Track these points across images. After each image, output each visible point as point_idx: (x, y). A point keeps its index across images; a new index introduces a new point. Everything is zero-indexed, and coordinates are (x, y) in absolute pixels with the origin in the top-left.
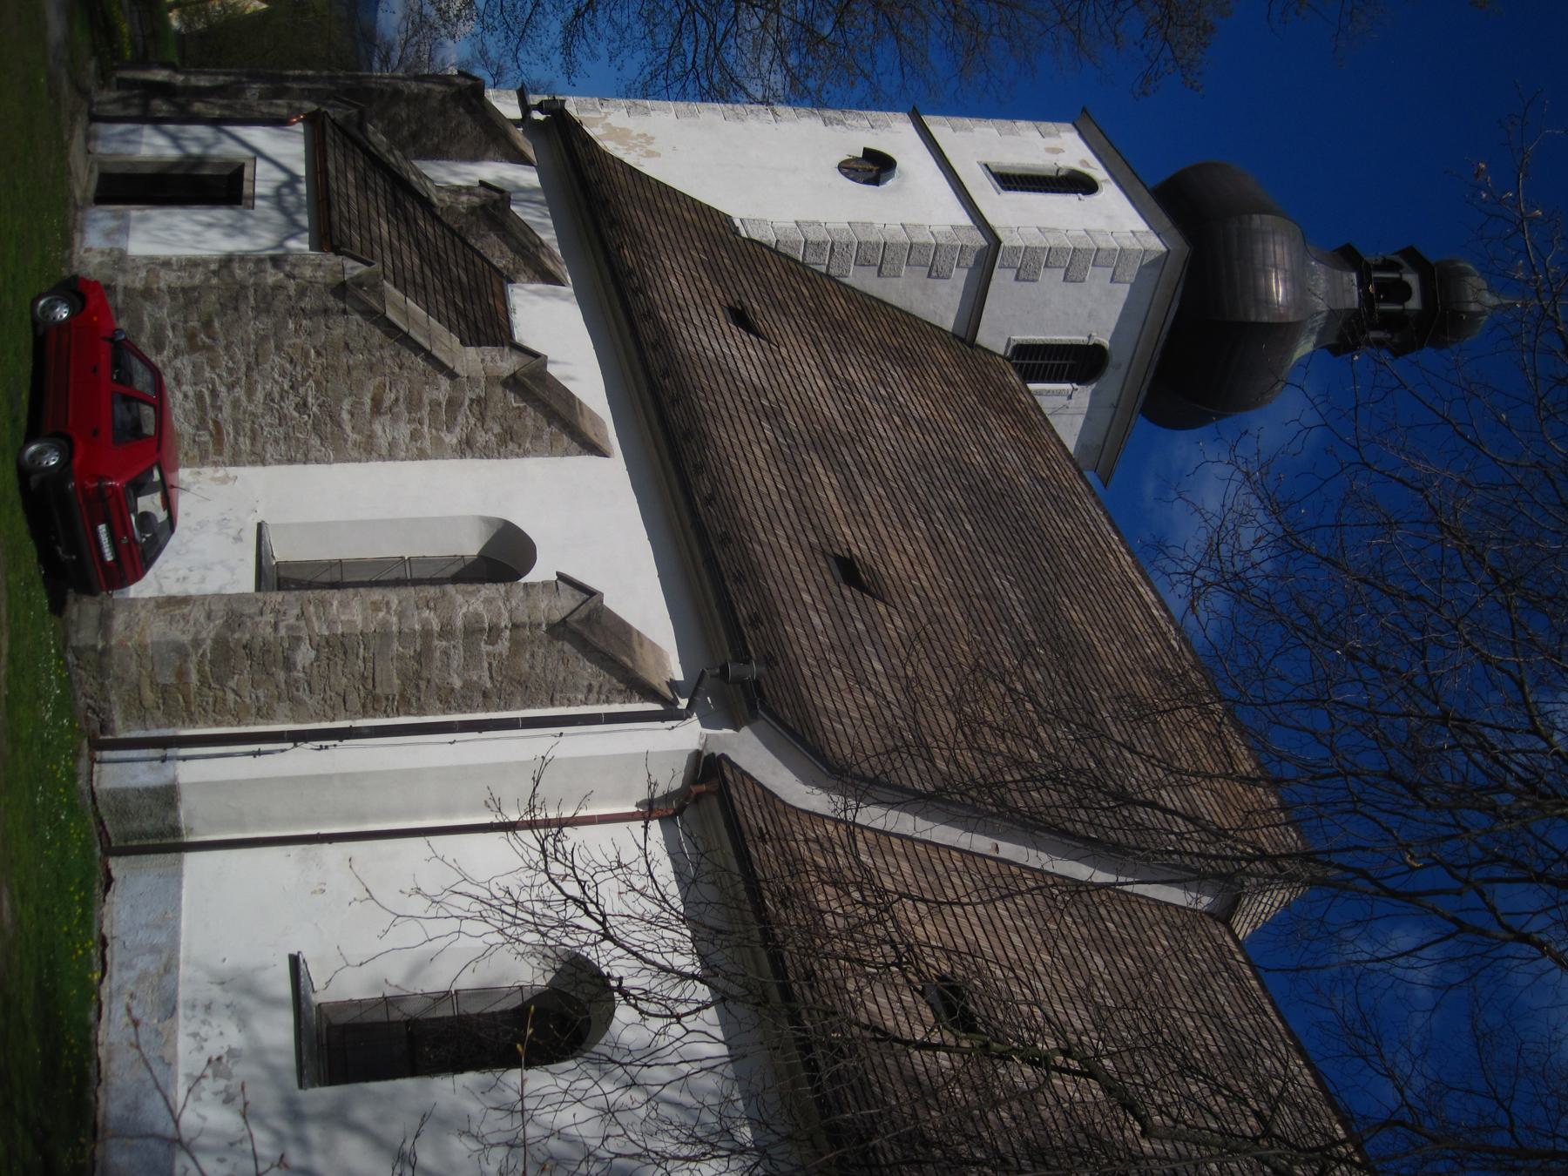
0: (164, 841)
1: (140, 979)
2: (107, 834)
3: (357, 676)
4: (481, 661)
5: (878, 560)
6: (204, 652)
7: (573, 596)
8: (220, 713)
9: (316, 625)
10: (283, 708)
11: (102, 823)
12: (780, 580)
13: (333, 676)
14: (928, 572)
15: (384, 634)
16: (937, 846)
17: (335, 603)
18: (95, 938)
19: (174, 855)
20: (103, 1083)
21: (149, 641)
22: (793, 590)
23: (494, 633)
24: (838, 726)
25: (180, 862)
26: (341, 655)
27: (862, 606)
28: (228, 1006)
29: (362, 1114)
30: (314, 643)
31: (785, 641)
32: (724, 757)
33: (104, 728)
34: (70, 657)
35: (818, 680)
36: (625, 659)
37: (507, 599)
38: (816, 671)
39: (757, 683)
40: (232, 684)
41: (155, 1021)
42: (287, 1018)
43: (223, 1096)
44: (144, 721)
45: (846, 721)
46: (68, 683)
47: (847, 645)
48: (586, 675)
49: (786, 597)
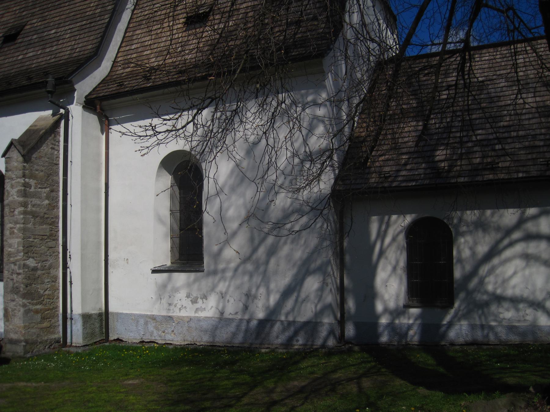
0: (104, 319)
1: (157, 329)
2: (100, 340)
3: (41, 242)
4: (38, 192)
5: (5, 26)
6: (28, 303)
7: (12, 151)
8: (54, 297)
9: (19, 258)
10: (52, 271)
11: (95, 343)
12: (11, 68)
13: (41, 252)
14: (13, 6)
15: (24, 230)
16: (131, 18)
17: (10, 249)
18: (141, 345)
19: (109, 316)
20: (196, 343)
21: (22, 325)
22: (17, 62)
23: (26, 185)
24: (78, 50)
25: (112, 313)
26: (32, 248)
27: (26, 35)
28: (170, 297)
29: (215, 248)
30: (27, 258)
31: (39, 67)
32: (86, 97)
33: (58, 341)
34: (28, 355)
35: (57, 56)
36: (41, 133)
37: (12, 179)
38: (53, 57)
39: (56, 79)
40: (42, 292)
41: (174, 324)
42: (176, 275)
43: (204, 300)
44: (56, 326)
45: (75, 47)
46: (39, 357)
47: (42, 43)
48: (47, 149)
49: (20, 65)
